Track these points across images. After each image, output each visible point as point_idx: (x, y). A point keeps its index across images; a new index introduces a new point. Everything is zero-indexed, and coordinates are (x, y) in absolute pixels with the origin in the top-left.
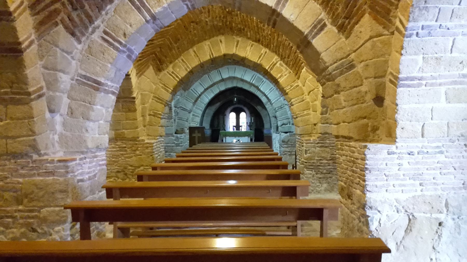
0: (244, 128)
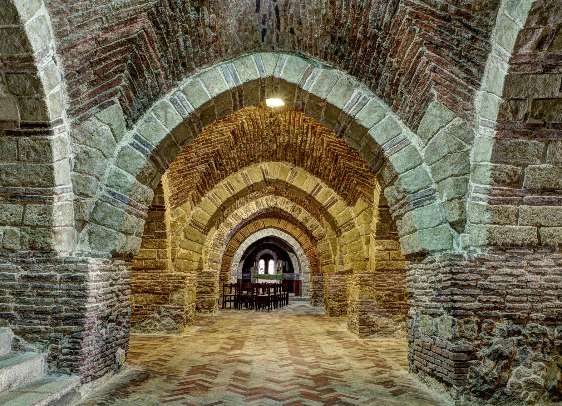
0: (271, 271)
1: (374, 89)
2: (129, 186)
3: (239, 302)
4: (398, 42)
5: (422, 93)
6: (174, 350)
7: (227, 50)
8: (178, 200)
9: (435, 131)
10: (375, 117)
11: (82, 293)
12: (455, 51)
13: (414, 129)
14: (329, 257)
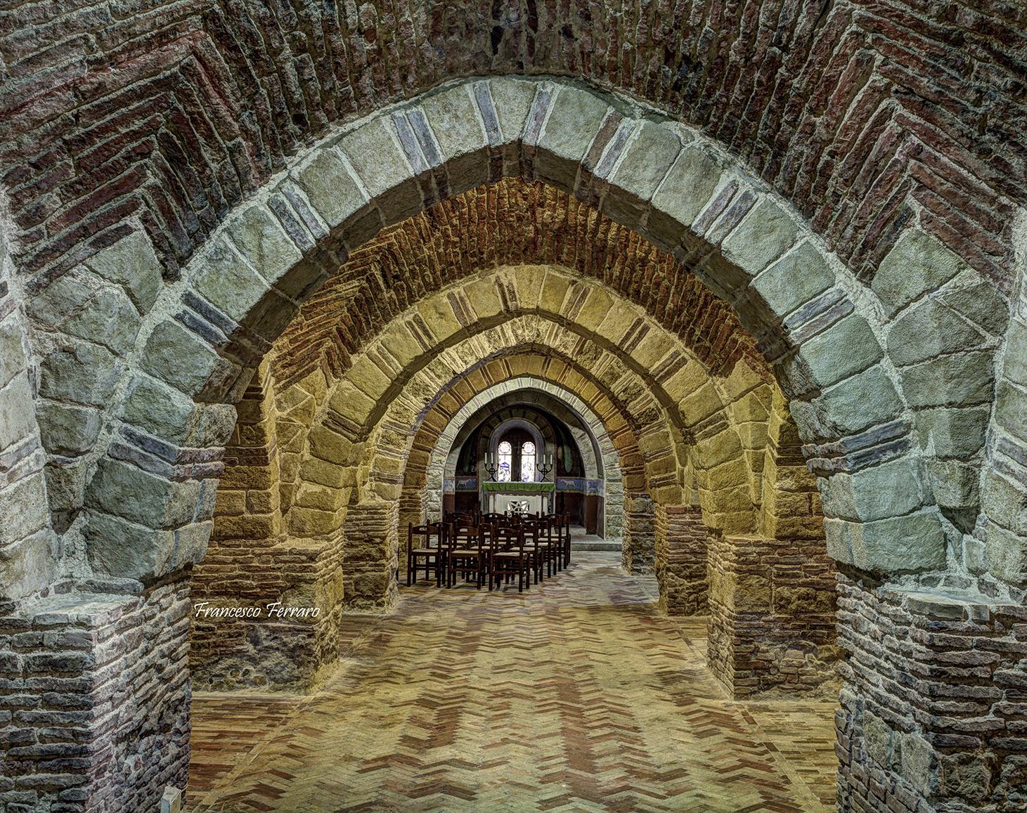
0: (529, 472)
1: (770, 176)
2: (177, 421)
3: (446, 570)
4: (831, 83)
5: (884, 202)
6: (294, 753)
7: (404, 78)
8: (294, 368)
9: (913, 295)
10: (769, 243)
11: (80, 698)
12: (970, 116)
13: (863, 276)
14: (669, 466)
